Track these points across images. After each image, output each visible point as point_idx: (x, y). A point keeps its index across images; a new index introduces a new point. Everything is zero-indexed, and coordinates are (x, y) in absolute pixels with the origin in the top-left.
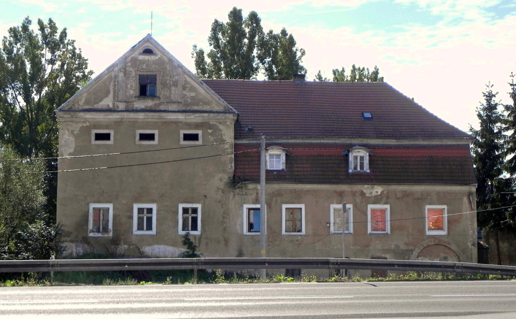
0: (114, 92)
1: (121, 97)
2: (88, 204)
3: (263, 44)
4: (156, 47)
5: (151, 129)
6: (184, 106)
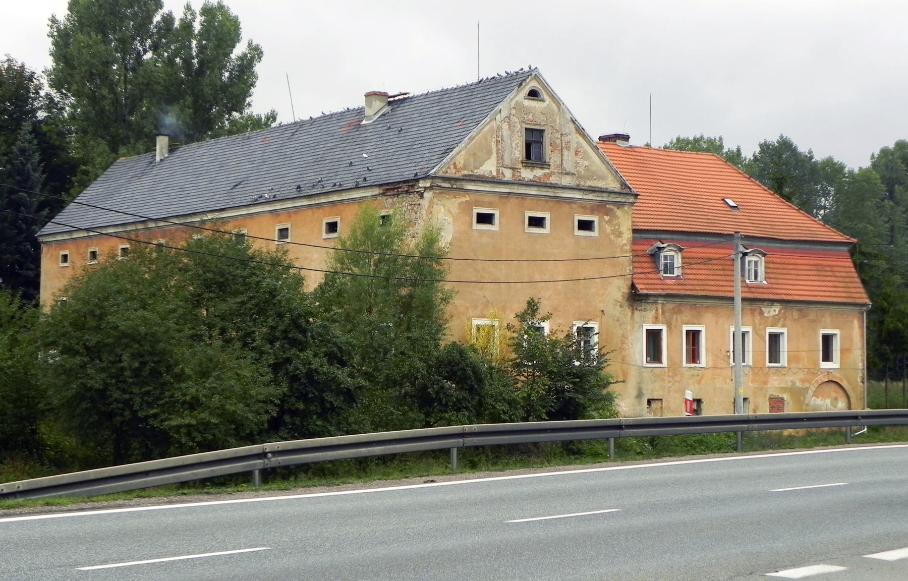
0: (498, 150)
2: (469, 319)
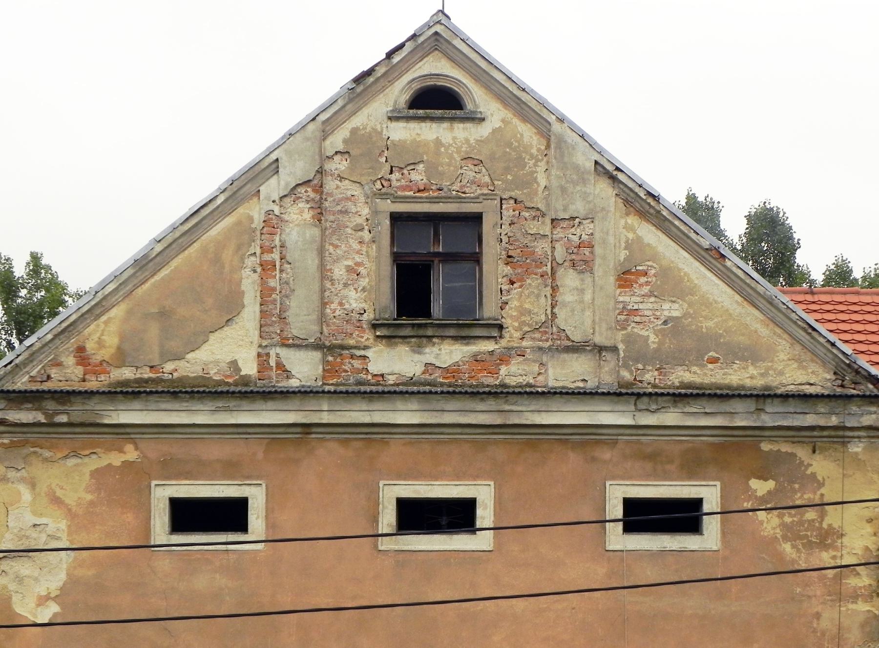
1: (301, 320)
3: (158, 499)
4: (463, 338)
5: (458, 476)
6: (626, 366)
